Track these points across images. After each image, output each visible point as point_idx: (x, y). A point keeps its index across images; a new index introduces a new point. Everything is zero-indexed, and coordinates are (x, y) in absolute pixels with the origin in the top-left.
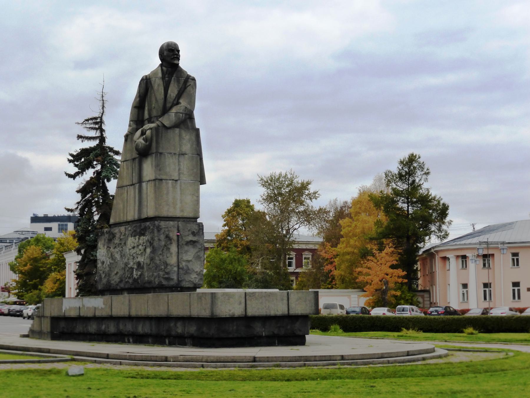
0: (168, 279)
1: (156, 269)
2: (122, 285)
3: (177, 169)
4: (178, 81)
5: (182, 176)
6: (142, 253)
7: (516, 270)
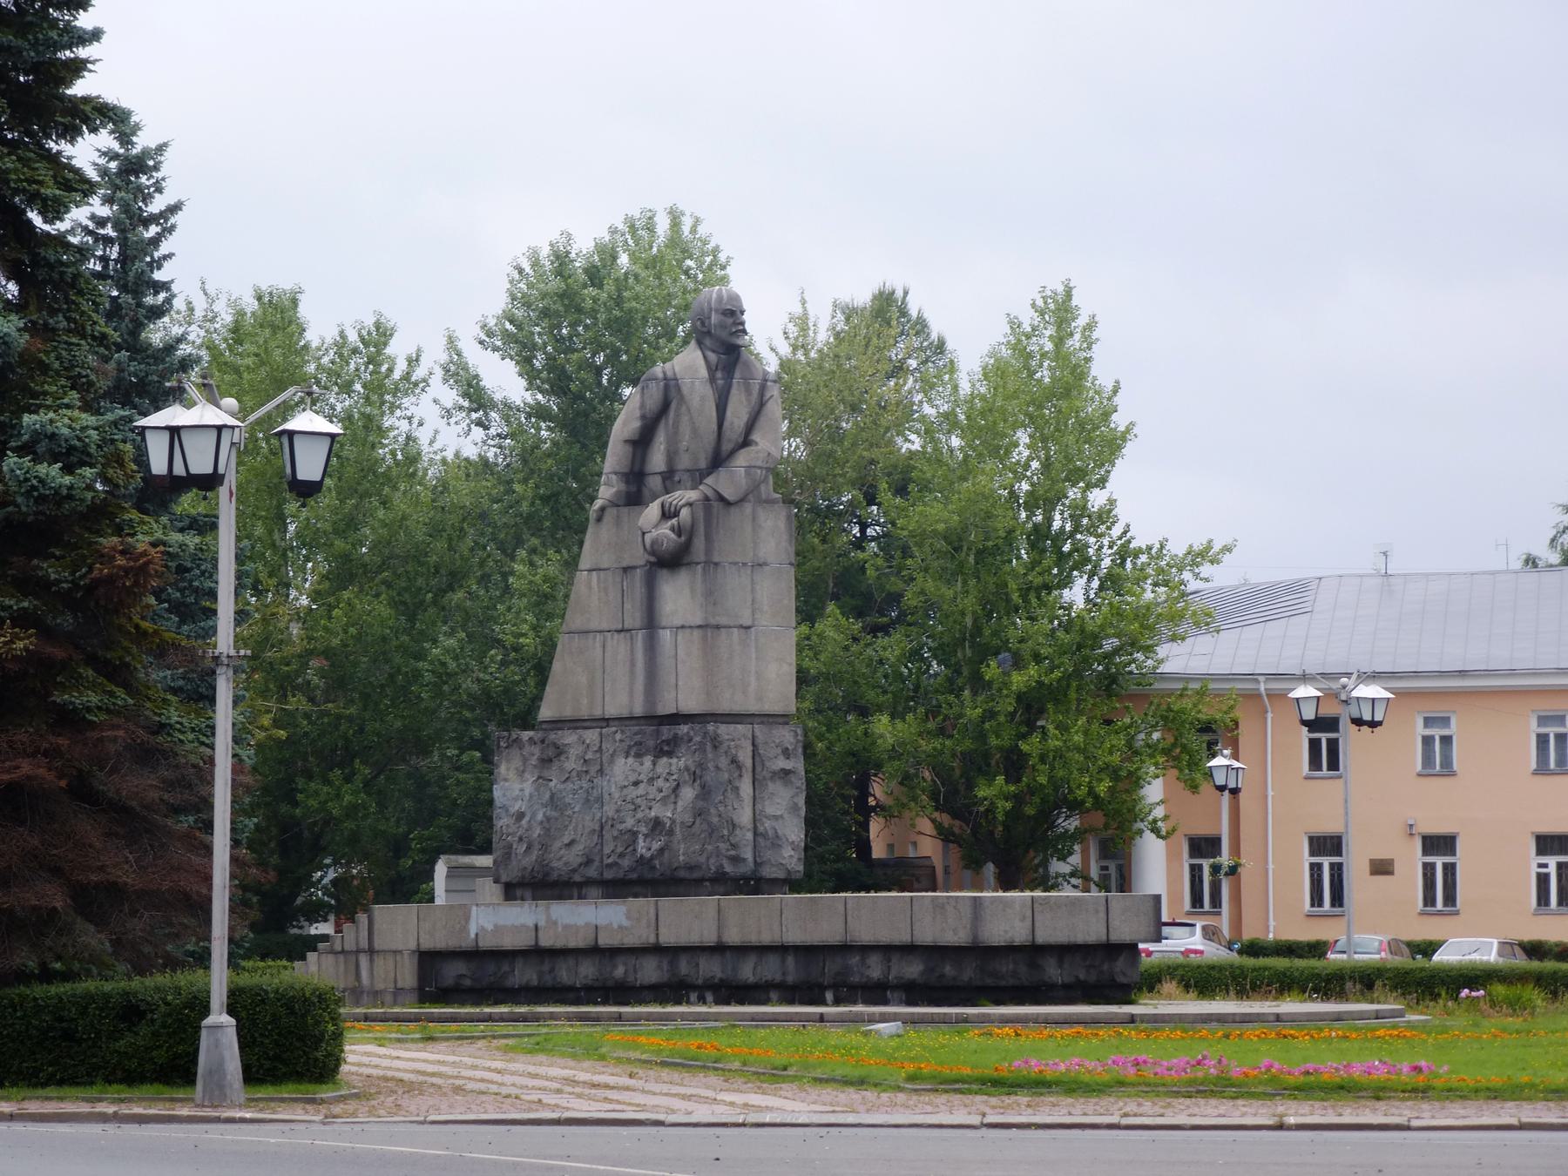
0: (736, 860)
1: (710, 835)
2: (592, 872)
3: (749, 599)
4: (748, 391)
6: (664, 799)
7: (1327, 789)
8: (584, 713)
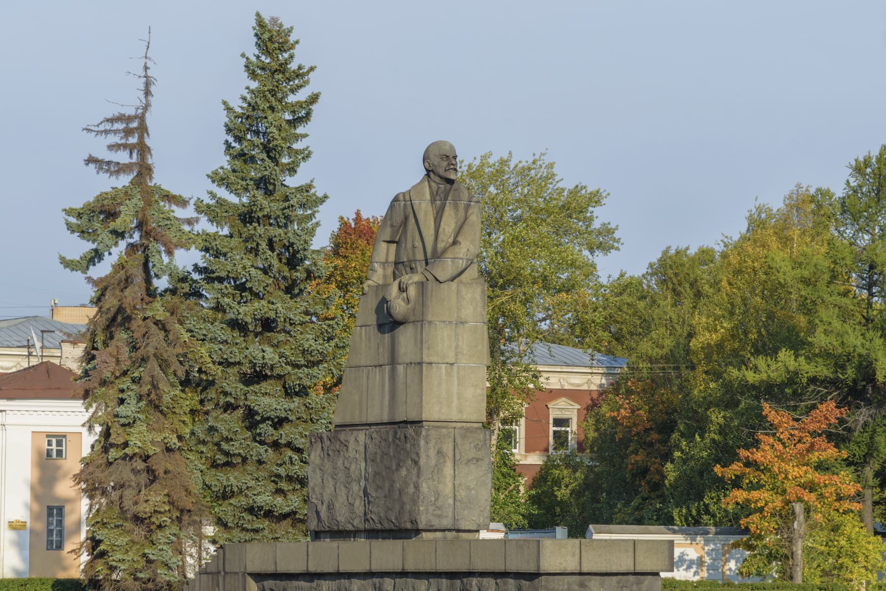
3: (454, 345)
4: (456, 207)
5: (460, 356)
8: (357, 420)
